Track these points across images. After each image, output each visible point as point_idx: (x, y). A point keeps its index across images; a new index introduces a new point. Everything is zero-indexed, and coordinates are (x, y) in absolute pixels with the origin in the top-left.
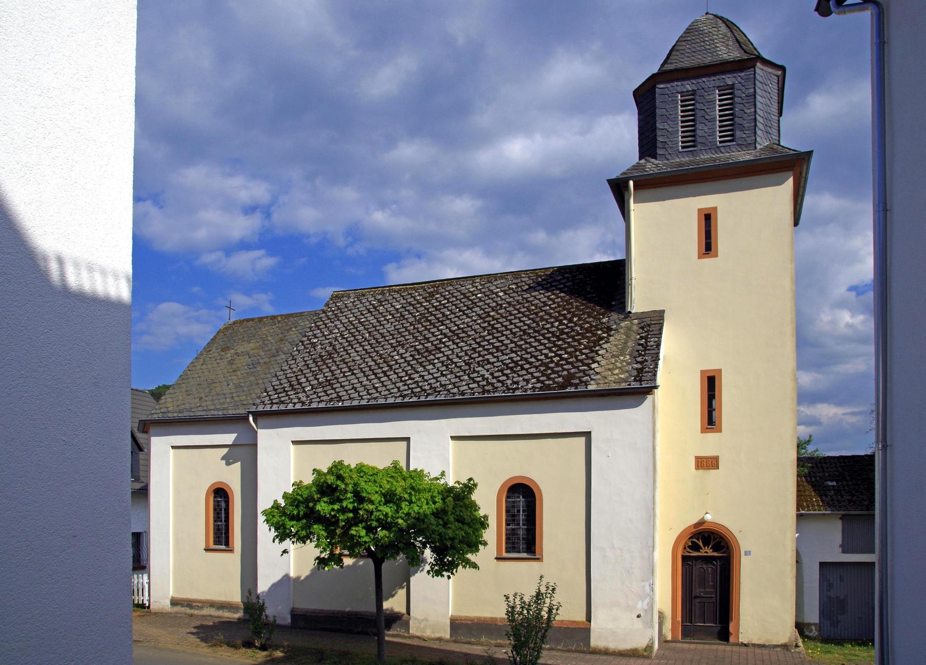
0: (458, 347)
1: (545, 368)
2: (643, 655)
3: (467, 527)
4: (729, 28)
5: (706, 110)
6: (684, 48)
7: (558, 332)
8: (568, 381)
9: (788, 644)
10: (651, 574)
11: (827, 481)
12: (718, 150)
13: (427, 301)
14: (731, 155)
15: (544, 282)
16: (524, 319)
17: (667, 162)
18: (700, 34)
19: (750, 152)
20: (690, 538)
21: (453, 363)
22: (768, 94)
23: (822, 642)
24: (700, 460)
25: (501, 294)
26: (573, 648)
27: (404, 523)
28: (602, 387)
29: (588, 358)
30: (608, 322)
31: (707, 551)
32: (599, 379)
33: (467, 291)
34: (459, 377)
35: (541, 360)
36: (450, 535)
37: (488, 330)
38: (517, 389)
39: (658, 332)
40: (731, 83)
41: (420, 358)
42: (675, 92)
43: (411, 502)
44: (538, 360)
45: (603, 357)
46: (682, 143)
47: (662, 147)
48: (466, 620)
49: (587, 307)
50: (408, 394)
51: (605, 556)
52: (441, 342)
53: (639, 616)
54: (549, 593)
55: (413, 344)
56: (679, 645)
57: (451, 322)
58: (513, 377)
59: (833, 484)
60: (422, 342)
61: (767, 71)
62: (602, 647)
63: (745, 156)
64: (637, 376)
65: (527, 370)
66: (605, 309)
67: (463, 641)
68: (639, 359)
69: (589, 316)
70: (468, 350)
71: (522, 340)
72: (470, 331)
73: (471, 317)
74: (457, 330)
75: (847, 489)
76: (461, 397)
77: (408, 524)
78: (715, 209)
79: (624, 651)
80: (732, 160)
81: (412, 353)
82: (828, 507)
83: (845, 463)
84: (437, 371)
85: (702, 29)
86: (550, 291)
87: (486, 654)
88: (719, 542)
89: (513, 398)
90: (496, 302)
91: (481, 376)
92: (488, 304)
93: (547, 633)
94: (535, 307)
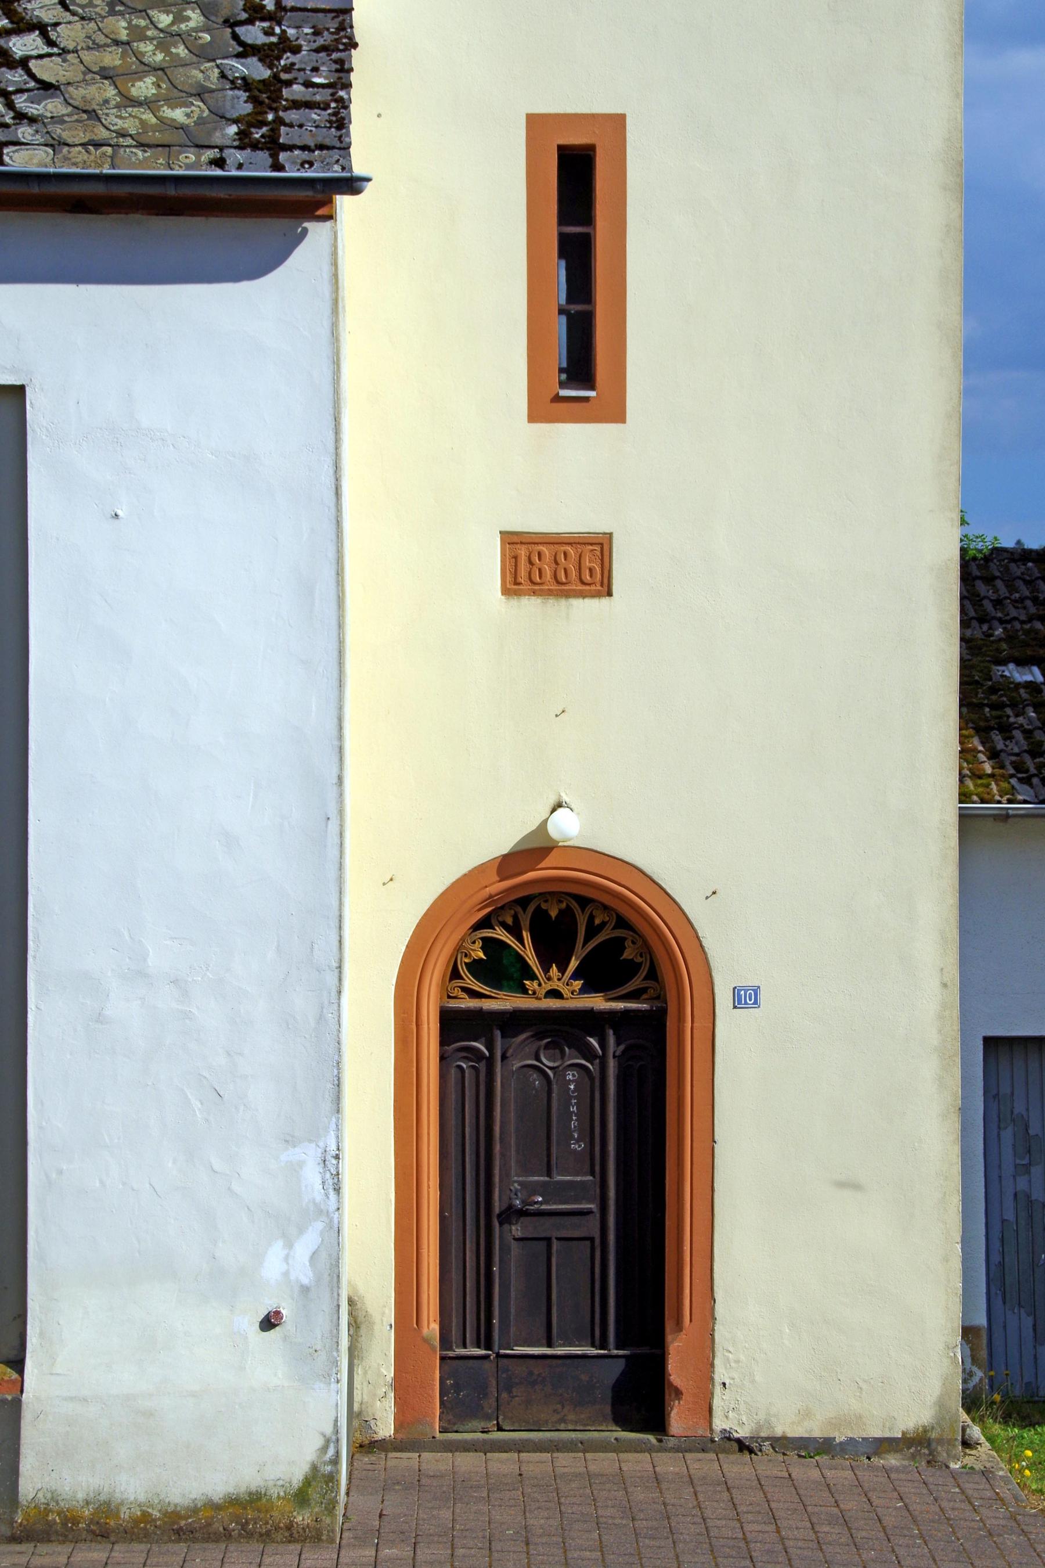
2: (289, 1527)
9: (934, 1435)
10: (327, 1106)
11: (1004, 662)
23: (1006, 1419)
24: (523, 552)
51: (100, 1018)
53: (269, 1322)
56: (434, 1462)
59: (1028, 678)
62: (81, 1496)
64: (255, 121)
68: (254, 34)
79: (195, 1510)
82: (1020, 780)
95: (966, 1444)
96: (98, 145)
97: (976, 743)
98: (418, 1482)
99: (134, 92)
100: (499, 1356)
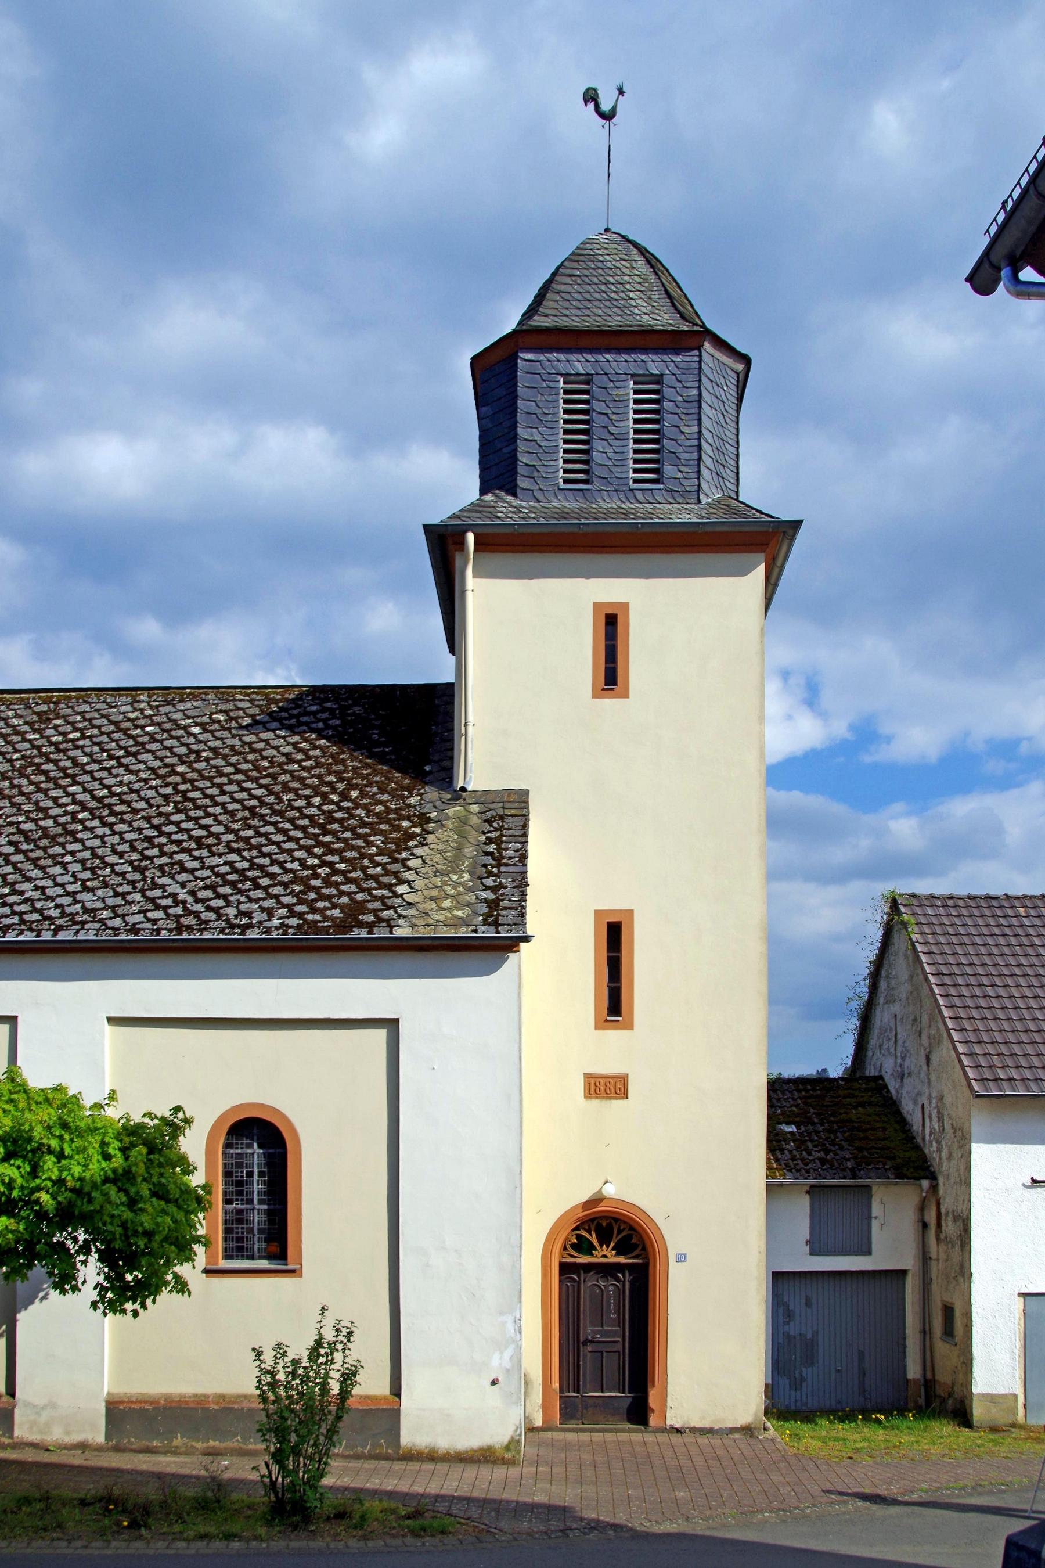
0: (114, 833)
1: (302, 888)
2: (503, 1459)
3: (175, 1209)
4: (652, 267)
5: (610, 416)
6: (569, 289)
7: (322, 817)
8: (353, 915)
9: (753, 1426)
11: (780, 1123)
12: (630, 494)
13: (35, 731)
14: (654, 509)
15: (284, 714)
16: (248, 785)
17: (536, 505)
18: (599, 268)
19: (688, 507)
20: (574, 1230)
21: (107, 865)
22: (721, 404)
24: (592, 1081)
25: (196, 730)
26: (366, 1451)
27: (51, 1202)
28: (422, 932)
29: (387, 873)
30: (421, 804)
31: (606, 1255)
32: (413, 916)
33: (121, 717)
34: (123, 895)
35: (291, 871)
36: (146, 1224)
37: (176, 803)
38: (249, 926)
39: (521, 833)
40: (658, 372)
41: (32, 851)
42: (554, 371)
43: (61, 1156)
44: (287, 871)
45: (417, 873)
46: (564, 473)
47: (526, 474)
48: (140, 1402)
49: (376, 772)
50: (13, 924)
51: (427, 1265)
52: (74, 819)
53: (494, 1383)
54: (342, 1342)
55: (13, 819)
56: (558, 1436)
57: (94, 779)
58: (239, 903)
60: (33, 815)
61: (721, 359)
62: (424, 1445)
63: (681, 514)
64: (489, 915)
65: (265, 889)
66: (413, 778)
67: (134, 1447)
68: (489, 882)
69: (382, 790)
70: (136, 840)
71: (249, 827)
72: (136, 801)
73: (136, 773)
74: (107, 797)
75: (816, 1138)
76: (131, 937)
77: (59, 1203)
78: (625, 606)
79: (467, 1452)
80: (658, 517)
81: (14, 838)
82: (788, 1170)
83: (807, 1091)
84: (72, 880)
85: (601, 259)
86: (298, 734)
87: (203, 1473)
88: (629, 1237)
89: (242, 944)
90: (187, 745)
91: (170, 895)
92: (170, 749)
93: (340, 1425)
94: (270, 762)
95: (765, 1429)
96: (429, 926)
97: (770, 1155)
98: (552, 1443)
99: (443, 905)
100: (582, 1396)
